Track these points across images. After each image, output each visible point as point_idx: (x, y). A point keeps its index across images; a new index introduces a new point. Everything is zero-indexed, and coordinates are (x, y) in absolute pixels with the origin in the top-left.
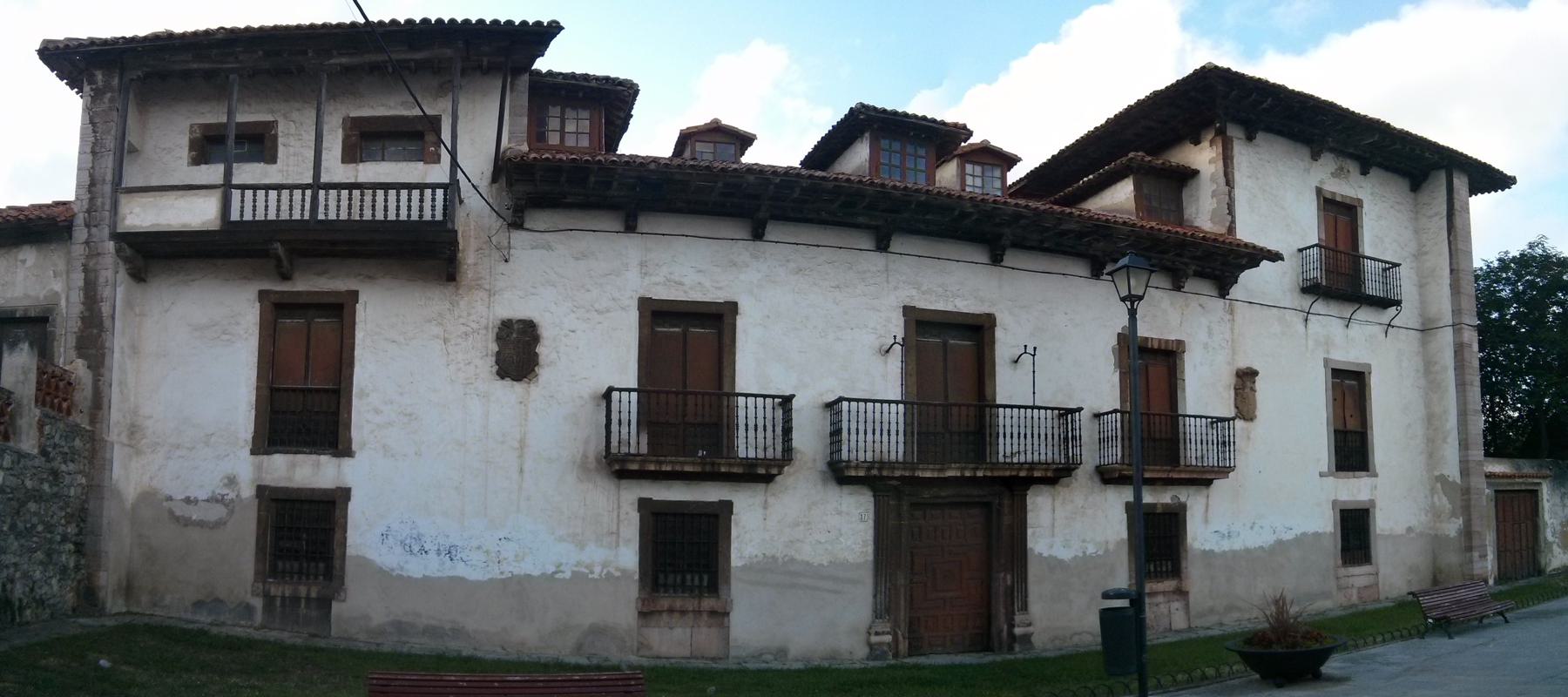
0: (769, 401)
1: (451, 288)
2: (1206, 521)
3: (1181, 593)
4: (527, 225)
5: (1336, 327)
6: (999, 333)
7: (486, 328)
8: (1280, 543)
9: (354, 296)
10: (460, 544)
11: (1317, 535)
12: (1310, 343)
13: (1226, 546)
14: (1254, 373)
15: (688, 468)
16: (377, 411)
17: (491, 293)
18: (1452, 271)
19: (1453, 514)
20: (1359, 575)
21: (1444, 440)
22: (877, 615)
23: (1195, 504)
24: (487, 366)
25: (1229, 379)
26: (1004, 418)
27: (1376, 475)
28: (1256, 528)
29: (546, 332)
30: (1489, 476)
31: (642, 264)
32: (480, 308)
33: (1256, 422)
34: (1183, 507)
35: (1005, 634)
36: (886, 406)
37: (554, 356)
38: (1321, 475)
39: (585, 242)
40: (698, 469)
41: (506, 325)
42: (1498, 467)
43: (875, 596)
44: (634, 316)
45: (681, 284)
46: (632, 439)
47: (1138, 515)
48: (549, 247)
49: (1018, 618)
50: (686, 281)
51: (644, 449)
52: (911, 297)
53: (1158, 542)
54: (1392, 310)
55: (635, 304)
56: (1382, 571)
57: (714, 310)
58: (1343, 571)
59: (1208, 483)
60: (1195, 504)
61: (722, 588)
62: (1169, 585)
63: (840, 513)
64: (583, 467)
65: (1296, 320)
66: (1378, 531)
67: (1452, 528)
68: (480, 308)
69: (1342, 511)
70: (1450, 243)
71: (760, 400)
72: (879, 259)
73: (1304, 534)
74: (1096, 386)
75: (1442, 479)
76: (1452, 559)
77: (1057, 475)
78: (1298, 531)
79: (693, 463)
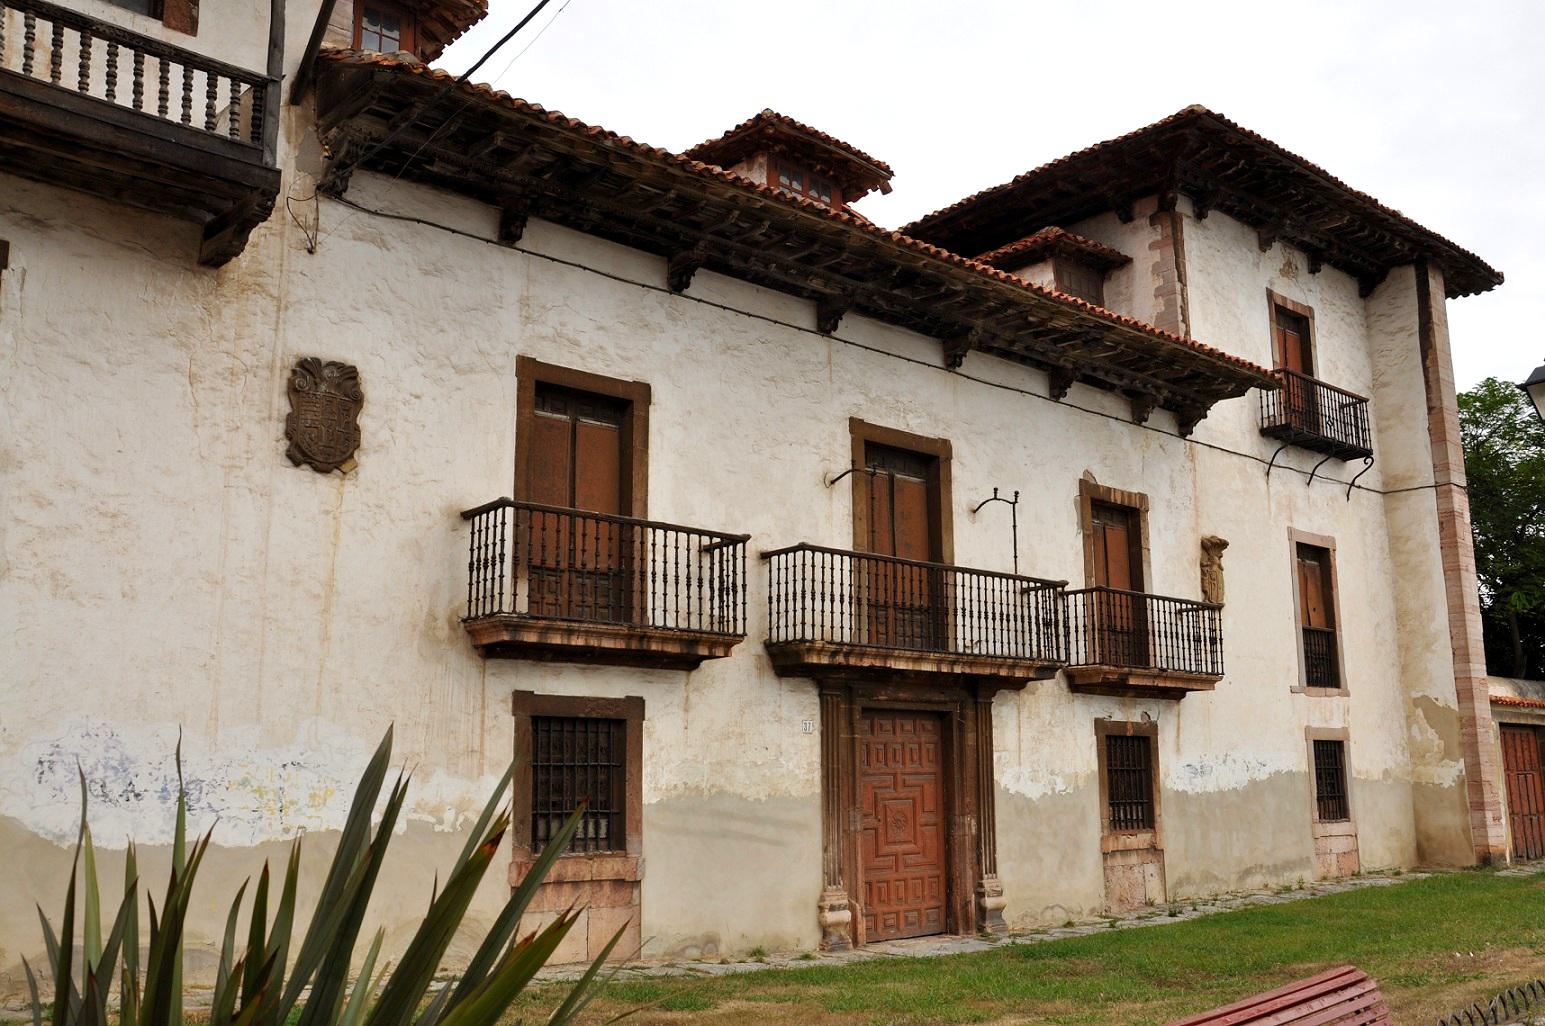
0: (694, 538)
1: (206, 282)
2: (1178, 750)
3: (1155, 851)
4: (348, 196)
5: (1296, 481)
6: (956, 469)
7: (271, 368)
8: (1254, 783)
10: (208, 777)
11: (1290, 773)
14: (1223, 545)
15: (607, 644)
16: (40, 501)
17: (281, 305)
18: (1430, 409)
19: (1447, 754)
21: (1428, 647)
22: (831, 878)
24: (271, 439)
25: (1195, 553)
26: (964, 592)
27: (1347, 695)
29: (372, 388)
30: (1495, 702)
31: (524, 302)
32: (261, 329)
34: (1154, 727)
35: (972, 907)
37: (384, 435)
39: (440, 246)
40: (620, 645)
41: (308, 369)
42: (1502, 689)
43: (825, 850)
44: (512, 383)
45: (577, 344)
46: (513, 597)
48: (383, 244)
49: (988, 883)
50: (583, 339)
51: (523, 606)
52: (858, 406)
53: (1129, 776)
54: (1356, 465)
57: (620, 393)
59: (1177, 695)
61: (631, 839)
62: (1142, 839)
63: (779, 720)
64: (429, 634)
65: (1256, 471)
67: (1449, 773)
68: (261, 329)
69: (1317, 743)
70: (1426, 369)
71: (683, 536)
72: (818, 343)
74: (1061, 552)
75: (1427, 705)
76: (1448, 820)
78: (1270, 769)
79: (615, 636)
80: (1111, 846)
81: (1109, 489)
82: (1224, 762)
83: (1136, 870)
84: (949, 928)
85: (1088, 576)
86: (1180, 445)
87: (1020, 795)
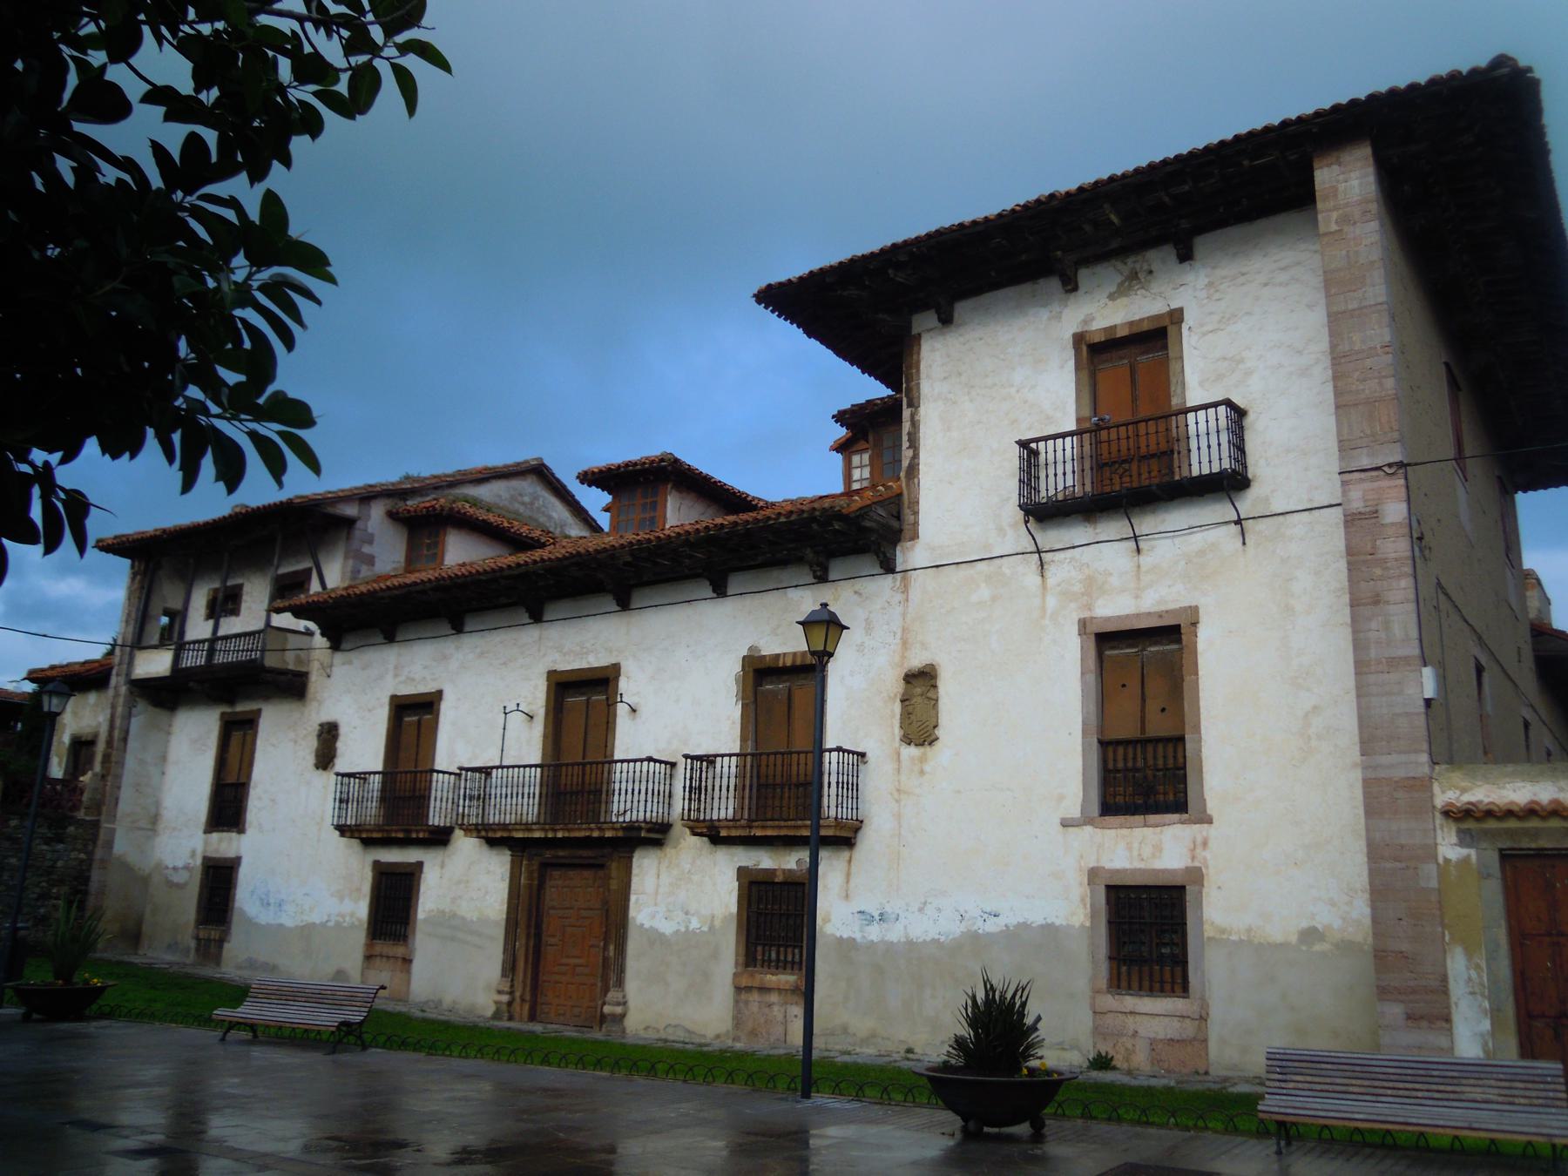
9: (259, 711)
12: (1051, 602)
13: (874, 933)
20: (1151, 1017)
23: (831, 871)
28: (929, 910)
29: (343, 730)
30: (1461, 816)
33: (938, 745)
36: (1211, 411)
38: (1066, 824)
47: (754, 887)
52: (555, 662)
53: (777, 924)
55: (386, 701)
56: (1216, 1013)
58: (1109, 1001)
60: (831, 871)
66: (1209, 932)
69: (1181, 889)
73: (1024, 926)
77: (655, 835)
78: (1009, 919)
80: (744, 982)
81: (778, 656)
82: (921, 910)
83: (776, 1008)
84: (532, 1017)
85: (743, 739)
86: (888, 581)
87: (653, 930)
